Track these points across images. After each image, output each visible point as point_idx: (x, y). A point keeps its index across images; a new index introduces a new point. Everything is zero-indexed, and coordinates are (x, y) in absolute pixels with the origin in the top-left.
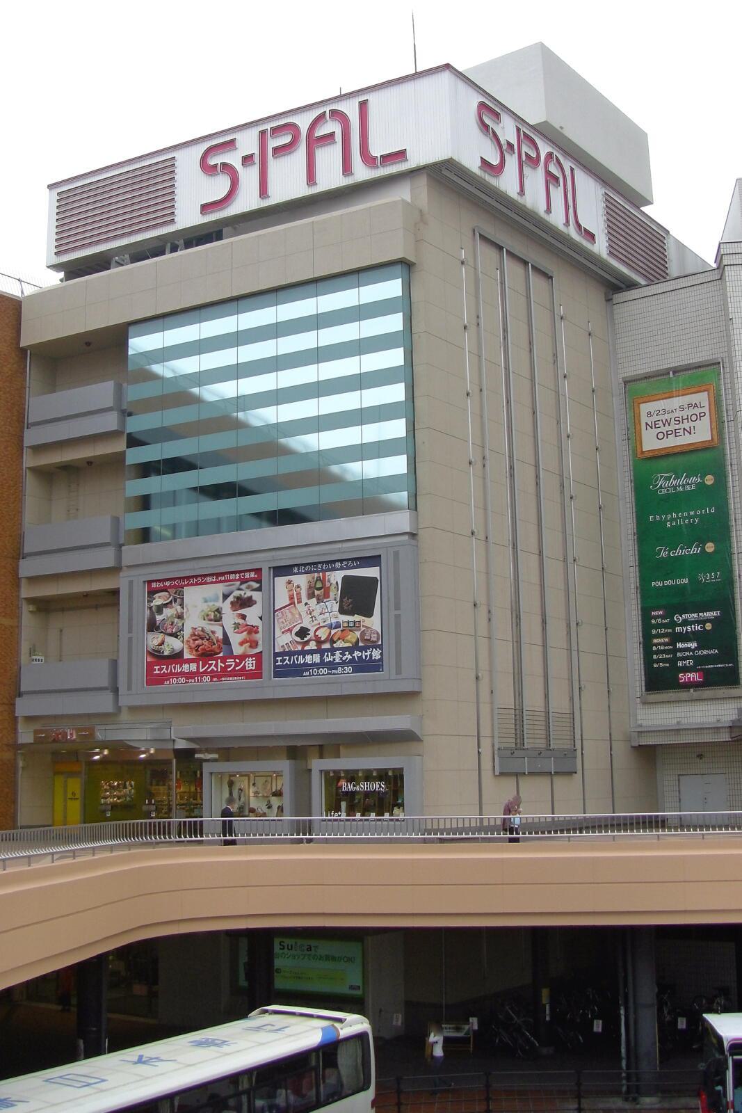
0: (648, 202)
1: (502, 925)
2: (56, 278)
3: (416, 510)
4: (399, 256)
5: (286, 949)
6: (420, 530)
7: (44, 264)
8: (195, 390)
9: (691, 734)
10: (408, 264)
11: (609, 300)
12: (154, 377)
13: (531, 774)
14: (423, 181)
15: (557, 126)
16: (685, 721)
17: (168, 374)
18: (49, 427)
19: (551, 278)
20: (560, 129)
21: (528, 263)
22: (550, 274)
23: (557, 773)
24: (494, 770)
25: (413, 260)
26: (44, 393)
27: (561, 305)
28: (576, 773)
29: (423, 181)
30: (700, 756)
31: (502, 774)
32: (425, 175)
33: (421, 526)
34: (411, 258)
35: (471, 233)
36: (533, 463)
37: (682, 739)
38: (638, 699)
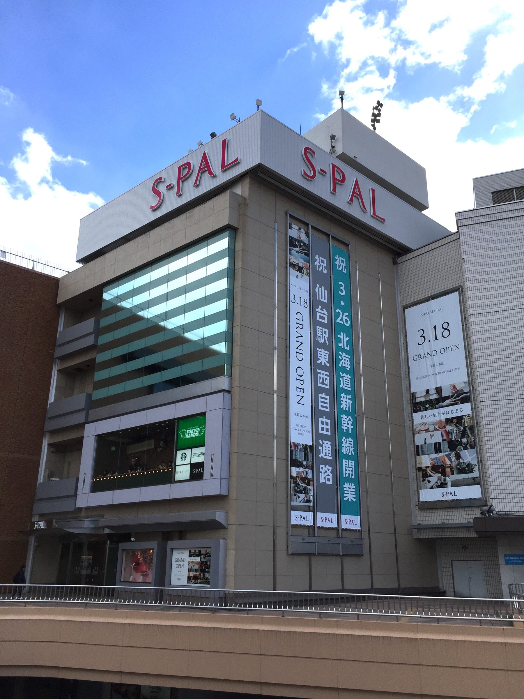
0: (426, 207)
1: (235, 692)
2: (80, 265)
3: (231, 376)
4: (226, 223)
5: (303, 599)
6: (232, 389)
7: (75, 260)
8: (162, 324)
9: (456, 531)
10: (234, 229)
11: (395, 263)
12: (141, 318)
13: (319, 555)
14: (247, 182)
15: (352, 156)
16: (447, 522)
17: (150, 316)
18: (76, 343)
19: (347, 245)
20: (354, 158)
21: (329, 235)
22: (348, 243)
23: (345, 555)
24: (288, 551)
25: (236, 226)
26: (73, 325)
27: (356, 262)
28: (363, 555)
29: (247, 182)
30: (465, 548)
31: (293, 554)
32: (248, 178)
33: (233, 386)
34: (235, 225)
35: (284, 214)
36: (284, 338)
37: (447, 535)
38: (417, 506)
